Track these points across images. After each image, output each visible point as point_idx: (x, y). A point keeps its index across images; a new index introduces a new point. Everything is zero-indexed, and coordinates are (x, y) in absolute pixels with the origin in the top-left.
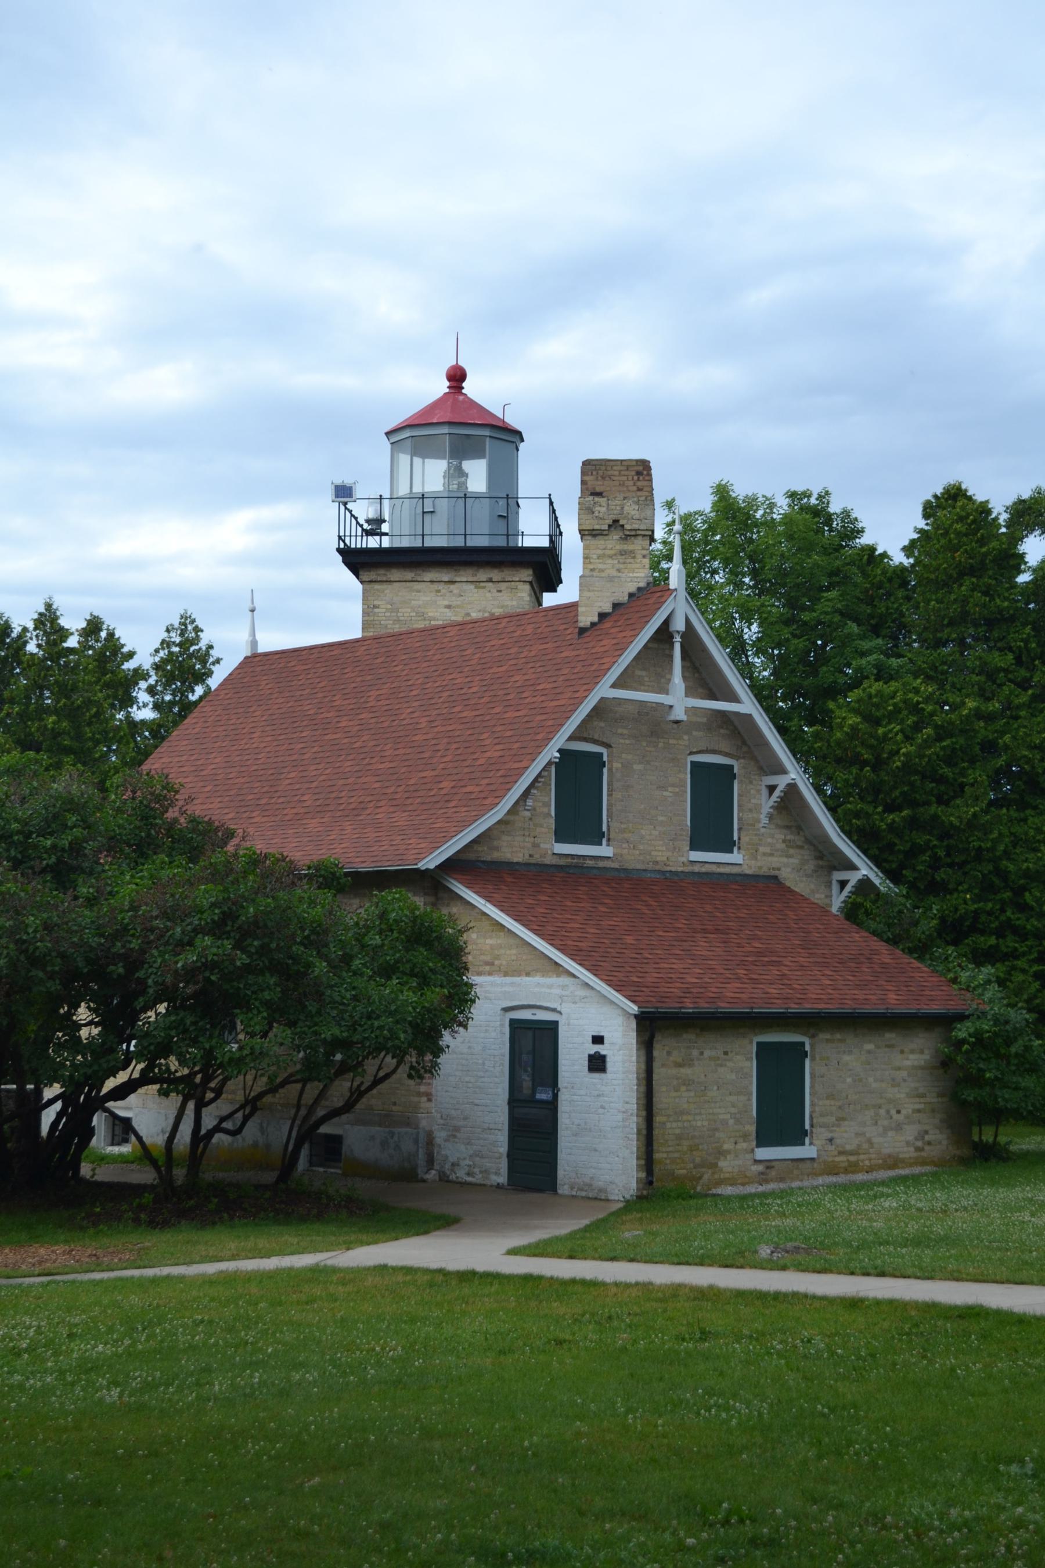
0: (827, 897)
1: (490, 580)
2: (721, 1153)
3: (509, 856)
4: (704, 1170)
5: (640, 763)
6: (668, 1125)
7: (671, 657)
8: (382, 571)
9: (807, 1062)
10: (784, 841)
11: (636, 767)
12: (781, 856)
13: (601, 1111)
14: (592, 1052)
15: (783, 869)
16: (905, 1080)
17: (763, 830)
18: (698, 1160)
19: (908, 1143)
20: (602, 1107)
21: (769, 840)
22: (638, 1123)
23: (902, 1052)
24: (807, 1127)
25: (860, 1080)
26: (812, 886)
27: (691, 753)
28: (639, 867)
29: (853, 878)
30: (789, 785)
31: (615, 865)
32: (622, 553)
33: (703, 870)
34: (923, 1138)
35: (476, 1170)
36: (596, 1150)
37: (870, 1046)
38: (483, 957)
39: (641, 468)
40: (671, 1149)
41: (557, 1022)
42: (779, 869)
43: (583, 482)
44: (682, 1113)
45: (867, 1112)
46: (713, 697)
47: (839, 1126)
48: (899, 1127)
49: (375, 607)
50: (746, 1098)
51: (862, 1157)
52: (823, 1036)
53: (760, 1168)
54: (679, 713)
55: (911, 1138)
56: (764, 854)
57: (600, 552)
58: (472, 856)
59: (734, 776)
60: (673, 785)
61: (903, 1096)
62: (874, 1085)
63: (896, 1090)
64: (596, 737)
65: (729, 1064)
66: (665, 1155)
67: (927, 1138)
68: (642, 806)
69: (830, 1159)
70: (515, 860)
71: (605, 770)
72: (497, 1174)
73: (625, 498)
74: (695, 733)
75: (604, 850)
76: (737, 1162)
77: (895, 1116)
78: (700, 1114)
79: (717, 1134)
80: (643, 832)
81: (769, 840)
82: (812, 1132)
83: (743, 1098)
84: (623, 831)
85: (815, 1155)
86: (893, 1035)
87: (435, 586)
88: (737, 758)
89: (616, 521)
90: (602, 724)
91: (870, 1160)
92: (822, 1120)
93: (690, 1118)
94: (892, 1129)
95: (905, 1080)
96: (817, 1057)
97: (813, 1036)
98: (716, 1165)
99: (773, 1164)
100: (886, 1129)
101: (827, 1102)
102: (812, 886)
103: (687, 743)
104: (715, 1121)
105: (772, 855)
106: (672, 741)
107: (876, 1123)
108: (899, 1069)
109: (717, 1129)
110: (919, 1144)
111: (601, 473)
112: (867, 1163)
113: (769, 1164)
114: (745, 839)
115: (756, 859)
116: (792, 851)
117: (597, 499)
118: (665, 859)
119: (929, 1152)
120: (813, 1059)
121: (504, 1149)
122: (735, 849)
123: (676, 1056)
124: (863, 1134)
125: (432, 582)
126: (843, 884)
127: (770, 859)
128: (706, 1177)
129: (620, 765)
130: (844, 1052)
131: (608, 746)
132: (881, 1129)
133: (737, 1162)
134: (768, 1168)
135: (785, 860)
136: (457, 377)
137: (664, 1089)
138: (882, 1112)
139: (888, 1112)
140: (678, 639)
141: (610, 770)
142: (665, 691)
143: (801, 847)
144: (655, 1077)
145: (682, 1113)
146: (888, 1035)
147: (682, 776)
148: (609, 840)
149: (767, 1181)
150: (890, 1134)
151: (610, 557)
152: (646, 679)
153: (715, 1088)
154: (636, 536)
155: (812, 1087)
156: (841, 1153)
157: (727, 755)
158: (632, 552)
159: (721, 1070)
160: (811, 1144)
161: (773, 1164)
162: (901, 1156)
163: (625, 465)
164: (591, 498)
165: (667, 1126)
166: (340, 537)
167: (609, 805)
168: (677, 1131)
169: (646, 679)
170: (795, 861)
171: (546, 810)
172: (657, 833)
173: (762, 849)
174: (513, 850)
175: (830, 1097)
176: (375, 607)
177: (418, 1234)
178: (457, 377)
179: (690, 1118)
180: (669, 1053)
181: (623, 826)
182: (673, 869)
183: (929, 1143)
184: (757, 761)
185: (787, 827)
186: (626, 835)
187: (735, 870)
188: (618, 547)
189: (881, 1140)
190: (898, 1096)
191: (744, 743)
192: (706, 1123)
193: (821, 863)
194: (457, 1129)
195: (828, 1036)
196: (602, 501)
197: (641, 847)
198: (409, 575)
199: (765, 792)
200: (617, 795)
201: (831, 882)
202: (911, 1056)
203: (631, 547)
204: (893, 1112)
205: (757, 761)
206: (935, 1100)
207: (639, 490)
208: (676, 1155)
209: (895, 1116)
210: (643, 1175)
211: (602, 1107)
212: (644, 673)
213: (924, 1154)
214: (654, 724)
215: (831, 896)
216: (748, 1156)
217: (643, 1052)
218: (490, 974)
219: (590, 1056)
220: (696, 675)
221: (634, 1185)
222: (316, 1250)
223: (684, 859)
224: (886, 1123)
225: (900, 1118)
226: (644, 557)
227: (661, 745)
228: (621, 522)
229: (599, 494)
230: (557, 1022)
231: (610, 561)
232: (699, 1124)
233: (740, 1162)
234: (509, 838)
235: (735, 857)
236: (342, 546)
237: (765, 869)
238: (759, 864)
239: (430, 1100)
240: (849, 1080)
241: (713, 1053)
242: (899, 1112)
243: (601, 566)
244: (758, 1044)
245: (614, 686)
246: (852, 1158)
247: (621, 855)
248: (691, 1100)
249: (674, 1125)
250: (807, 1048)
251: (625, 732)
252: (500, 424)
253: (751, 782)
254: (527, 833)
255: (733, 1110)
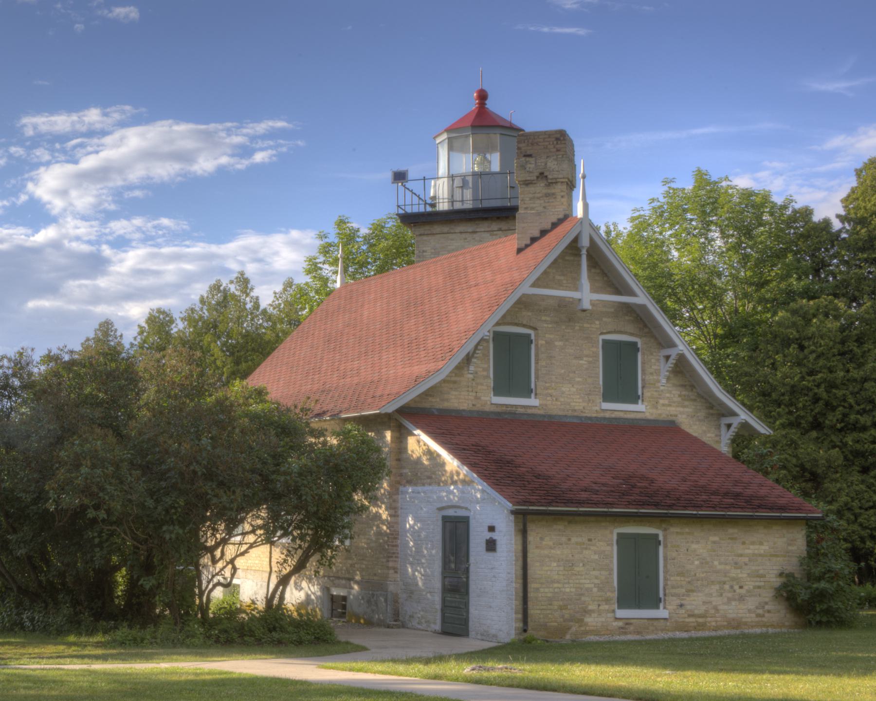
0: (716, 436)
1: (500, 230)
2: (587, 612)
3: (456, 405)
4: (572, 623)
5: (560, 340)
6: (542, 590)
7: (579, 265)
8: (427, 227)
9: (661, 548)
10: (680, 396)
11: (557, 343)
12: (677, 406)
13: (494, 579)
14: (488, 538)
15: (680, 416)
16: (746, 564)
17: (662, 388)
18: (567, 616)
19: (750, 611)
20: (494, 577)
21: (668, 395)
22: (516, 588)
23: (744, 543)
24: (661, 595)
25: (707, 563)
26: (704, 428)
27: (602, 333)
28: (560, 413)
29: (735, 422)
30: (678, 354)
31: (541, 412)
32: (547, 195)
33: (613, 416)
34: (763, 607)
35: (423, 621)
36: (491, 607)
37: (716, 539)
38: (426, 473)
39: (558, 136)
40: (544, 607)
41: (468, 517)
42: (676, 416)
43: (519, 148)
44: (553, 582)
45: (713, 587)
46: (618, 292)
47: (688, 596)
48: (741, 599)
49: (424, 251)
50: (607, 573)
51: (709, 619)
52: (673, 529)
53: (621, 624)
54: (586, 305)
55: (752, 607)
56: (663, 405)
57: (531, 196)
58: (427, 405)
59: (638, 350)
60: (587, 356)
61: (745, 575)
62: (720, 567)
63: (739, 571)
64: (525, 322)
65: (592, 548)
66: (539, 612)
67: (767, 607)
68: (563, 371)
69: (681, 620)
70: (461, 408)
71: (533, 346)
72: (435, 623)
73: (548, 157)
74: (604, 319)
75: (533, 401)
76: (600, 619)
77: (738, 591)
78: (569, 583)
79: (583, 598)
80: (563, 389)
81: (668, 395)
82: (665, 600)
83: (604, 573)
84: (547, 388)
85: (667, 617)
86: (736, 531)
87: (464, 236)
88: (640, 337)
89: (542, 174)
90: (530, 314)
91: (716, 622)
92: (674, 591)
93: (560, 585)
94: (735, 600)
95: (746, 564)
96: (669, 545)
97: (665, 530)
98: (581, 621)
99: (632, 621)
100: (730, 600)
101: (678, 578)
102: (704, 428)
103: (598, 326)
104: (581, 589)
105: (670, 405)
106: (585, 325)
107: (721, 595)
108: (741, 555)
109: (582, 595)
110: (760, 611)
111: (530, 141)
112: (714, 624)
113: (628, 622)
114: (647, 394)
115: (657, 408)
116: (686, 403)
117: (528, 159)
118: (581, 408)
119: (767, 618)
120: (665, 546)
121: (438, 606)
122: (640, 401)
123: (548, 541)
124: (710, 602)
125: (461, 233)
126: (729, 426)
127: (668, 408)
128: (574, 629)
129: (544, 342)
130: (693, 542)
131: (535, 329)
132: (725, 600)
133: (600, 619)
134: (627, 624)
135: (681, 409)
136: (483, 96)
137: (538, 564)
138: (727, 587)
139: (732, 587)
140: (584, 252)
141: (537, 345)
142: (576, 288)
143: (695, 400)
144: (530, 555)
145: (553, 582)
146: (731, 531)
147: (594, 349)
148: (536, 394)
149: (626, 633)
150: (733, 603)
151: (538, 198)
152: (565, 282)
153: (581, 565)
154: (556, 183)
155: (665, 566)
156: (689, 616)
157: (631, 334)
158: (553, 194)
159: (586, 552)
160: (665, 608)
161: (632, 621)
162: (744, 620)
163: (548, 135)
164: (523, 159)
165: (539, 592)
166: (398, 206)
167: (537, 370)
168: (549, 595)
169: (565, 282)
170: (689, 410)
171: (485, 373)
172: (575, 390)
173: (661, 402)
174: (459, 400)
175: (680, 574)
176: (424, 251)
177: (306, 657)
178: (483, 96)
179: (560, 585)
180: (542, 539)
181: (547, 385)
182: (589, 415)
183: (769, 612)
184: (656, 339)
185: (683, 386)
186: (550, 391)
187: (639, 416)
188: (545, 191)
189: (726, 607)
190: (740, 576)
191: (645, 326)
192: (573, 590)
193: (711, 411)
194: (412, 592)
195: (678, 530)
196: (532, 160)
197: (562, 400)
198: (445, 229)
199: (663, 360)
200: (542, 363)
201: (720, 425)
202: (751, 547)
203: (553, 191)
204: (736, 587)
205: (656, 339)
206: (774, 580)
207: (558, 150)
208: (548, 612)
209: (738, 591)
210: (521, 625)
211: (494, 577)
212: (562, 278)
213: (764, 619)
214: (568, 313)
215: (720, 436)
216: (610, 615)
217: (520, 538)
218: (430, 484)
219: (487, 540)
220: (605, 279)
221: (513, 632)
222: (171, 661)
223: (597, 408)
224: (730, 595)
225: (743, 591)
226: (562, 197)
227: (577, 328)
228: (546, 174)
229: (530, 156)
230: (468, 517)
231: (538, 201)
232: (568, 590)
233: (603, 619)
234: (457, 393)
235: (640, 407)
236: (401, 212)
237: (664, 416)
238: (659, 412)
239: (396, 572)
240: (697, 563)
241: (579, 540)
242: (741, 587)
243: (532, 205)
244: (619, 534)
245: (534, 285)
246: (701, 620)
247: (546, 405)
248: (560, 573)
249: (547, 590)
250: (661, 538)
251: (548, 319)
252: (508, 125)
253: (652, 354)
254: (470, 389)
255: (596, 581)
